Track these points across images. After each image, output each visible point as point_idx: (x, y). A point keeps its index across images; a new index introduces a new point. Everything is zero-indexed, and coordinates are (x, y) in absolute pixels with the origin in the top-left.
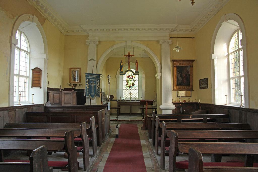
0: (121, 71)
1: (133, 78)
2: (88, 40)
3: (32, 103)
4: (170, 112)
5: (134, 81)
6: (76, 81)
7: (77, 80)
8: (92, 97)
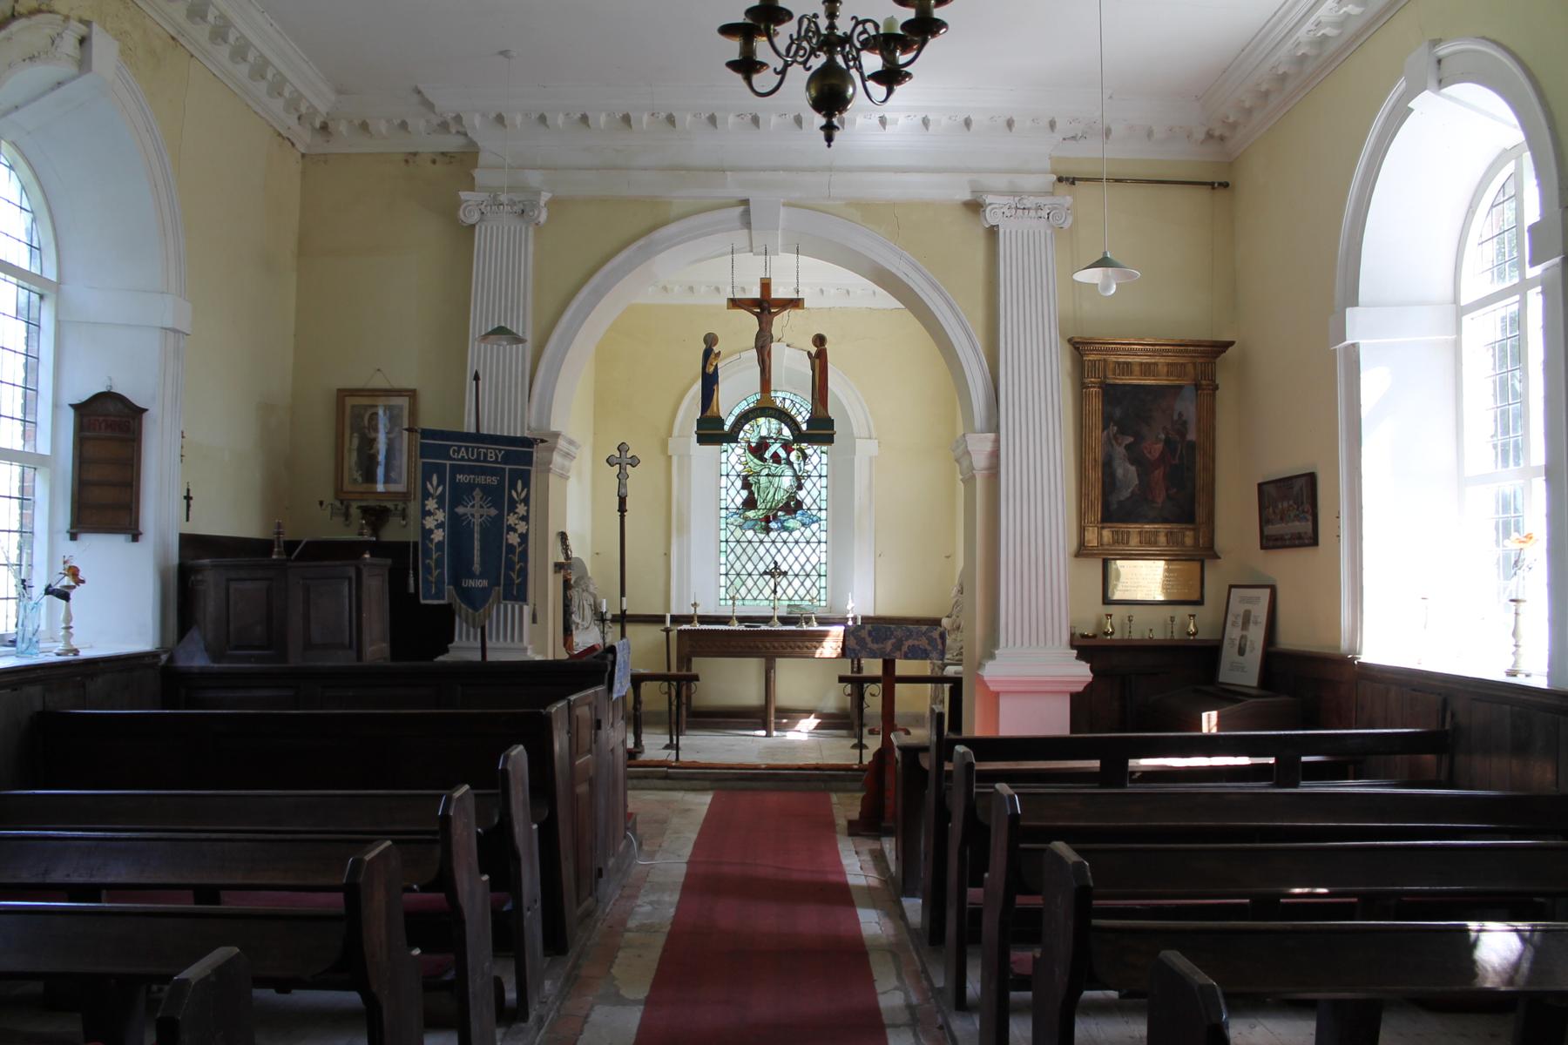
0: (709, 413)
1: (793, 456)
2: (471, 187)
3: (61, 646)
4: (1055, 721)
6: (380, 487)
7: (387, 480)
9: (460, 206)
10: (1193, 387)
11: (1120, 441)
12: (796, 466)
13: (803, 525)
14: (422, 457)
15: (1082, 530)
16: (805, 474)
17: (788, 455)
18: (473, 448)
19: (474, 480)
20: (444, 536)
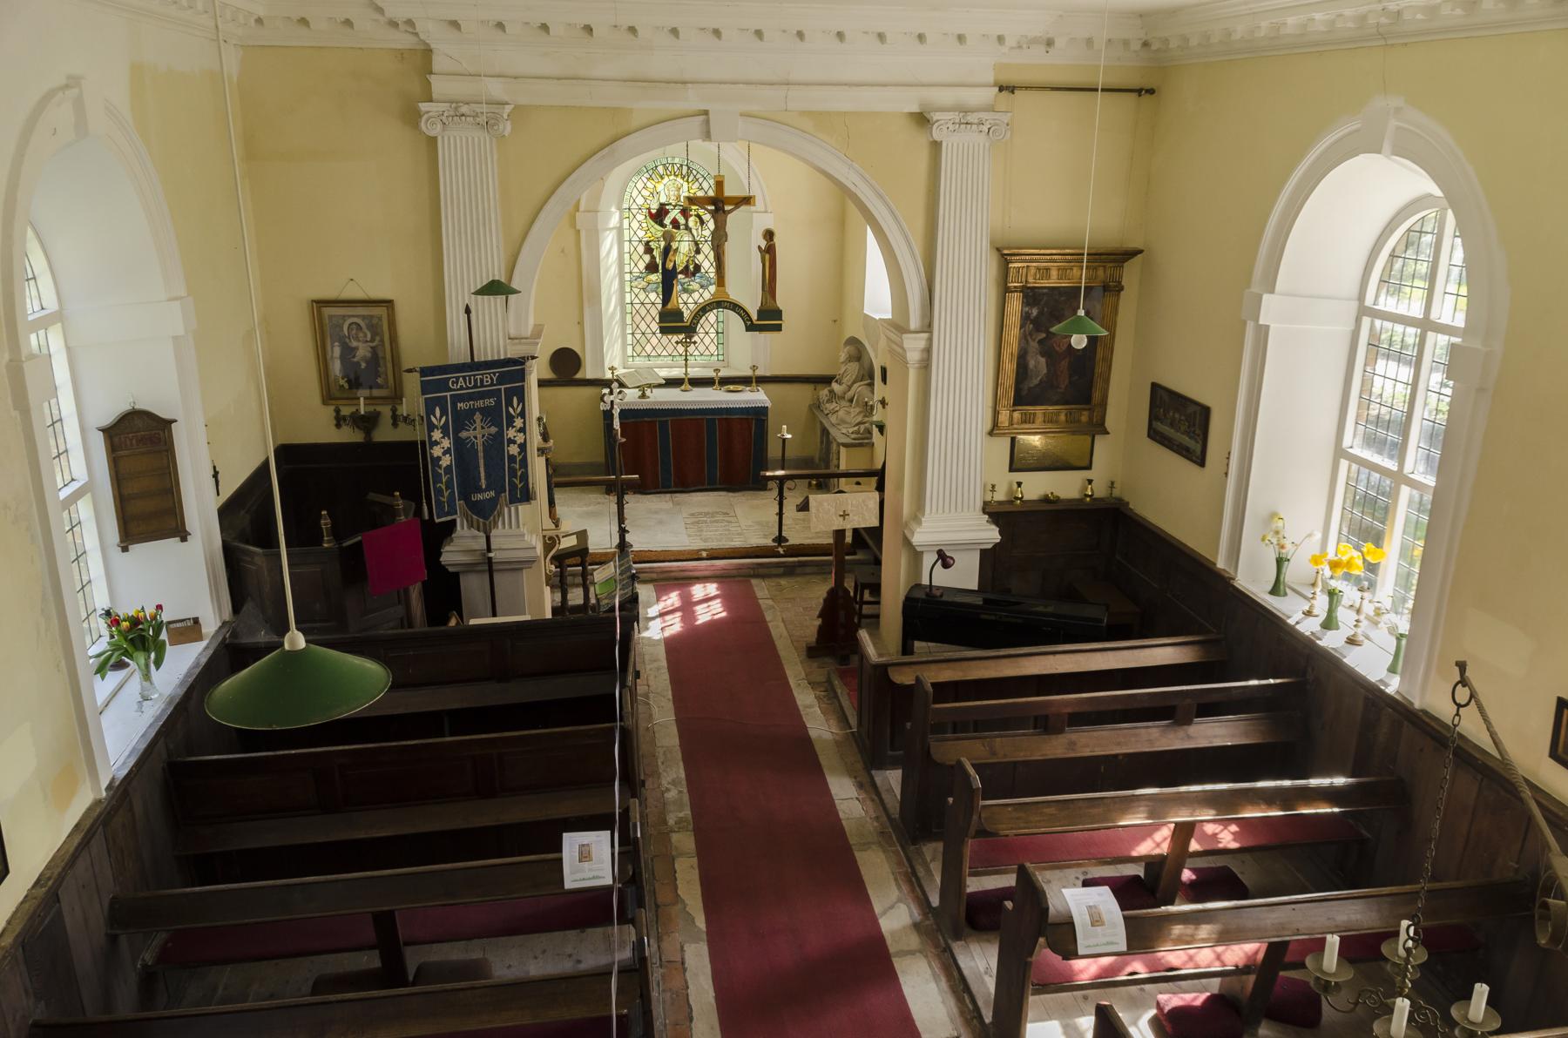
0: (669, 306)
1: (692, 222)
5: (696, 244)
8: (478, 514)
9: (421, 117)
10: (1101, 288)
11: (1034, 337)
12: (694, 232)
13: (702, 287)
14: (423, 394)
15: (996, 413)
16: (702, 239)
17: (687, 221)
18: (470, 376)
19: (474, 405)
20: (451, 460)
